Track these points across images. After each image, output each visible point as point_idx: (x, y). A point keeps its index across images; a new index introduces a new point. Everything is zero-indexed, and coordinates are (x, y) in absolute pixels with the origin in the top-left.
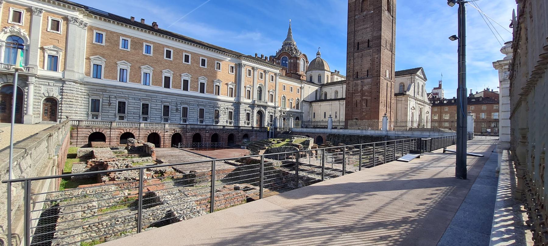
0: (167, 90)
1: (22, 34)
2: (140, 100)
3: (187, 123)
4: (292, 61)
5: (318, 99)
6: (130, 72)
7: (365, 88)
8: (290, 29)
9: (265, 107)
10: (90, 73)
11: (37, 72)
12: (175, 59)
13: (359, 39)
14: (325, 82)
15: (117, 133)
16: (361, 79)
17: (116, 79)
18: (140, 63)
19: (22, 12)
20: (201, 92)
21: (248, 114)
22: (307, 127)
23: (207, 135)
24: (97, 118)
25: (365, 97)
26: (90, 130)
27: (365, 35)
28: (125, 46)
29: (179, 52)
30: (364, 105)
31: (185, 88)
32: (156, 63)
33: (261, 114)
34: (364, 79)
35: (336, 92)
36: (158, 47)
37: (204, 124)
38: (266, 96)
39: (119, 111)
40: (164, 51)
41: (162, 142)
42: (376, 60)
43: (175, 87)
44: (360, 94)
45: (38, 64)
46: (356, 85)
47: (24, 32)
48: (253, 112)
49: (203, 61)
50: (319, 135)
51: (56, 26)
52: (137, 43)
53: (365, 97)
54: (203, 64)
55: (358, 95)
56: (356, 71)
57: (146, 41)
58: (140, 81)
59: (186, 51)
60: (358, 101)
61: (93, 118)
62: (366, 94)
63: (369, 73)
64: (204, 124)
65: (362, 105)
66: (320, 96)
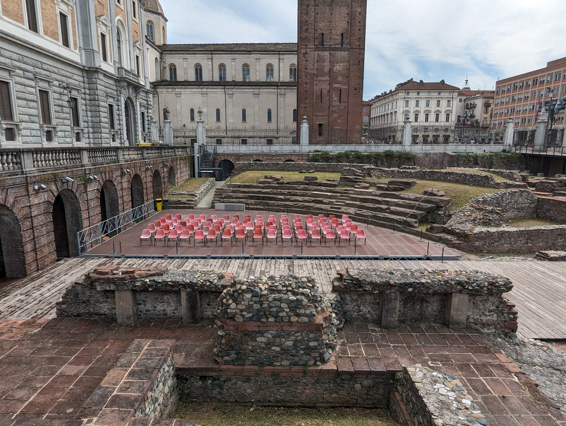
7: (338, 67)
13: (457, 300)
16: (330, 49)
25: (336, 85)
27: (423, 235)
30: (336, 98)
34: (336, 49)
35: (246, 68)
41: (28, 247)
42: (358, 18)
44: (327, 78)
46: (320, 60)
53: (336, 85)
55: (324, 79)
56: (319, 31)
60: (325, 92)
62: (340, 78)
63: (346, 41)
65: (330, 99)
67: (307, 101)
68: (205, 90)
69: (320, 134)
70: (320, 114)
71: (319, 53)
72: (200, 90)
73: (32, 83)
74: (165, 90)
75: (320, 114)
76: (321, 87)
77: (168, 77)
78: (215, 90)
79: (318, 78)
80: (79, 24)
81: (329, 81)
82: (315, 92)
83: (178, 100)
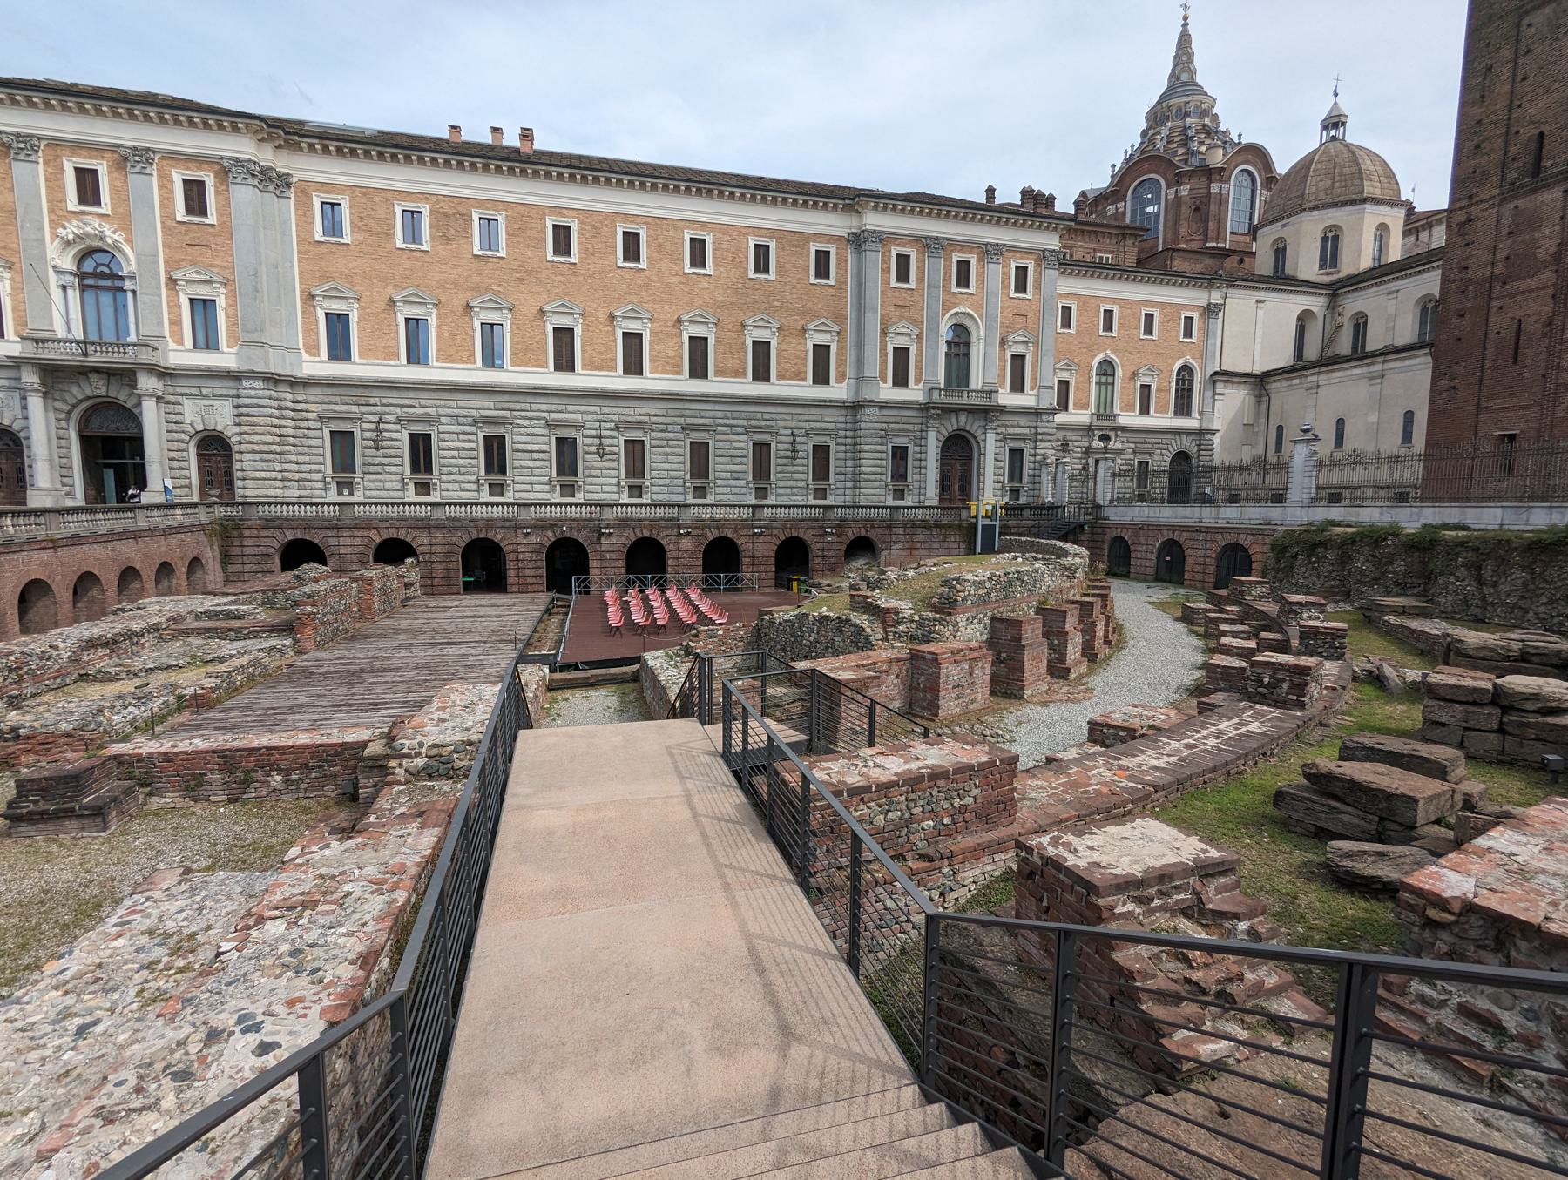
0: (760, 389)
1: (109, 241)
2: (475, 423)
3: (830, 501)
4: (1185, 190)
5: (1311, 353)
6: (439, 327)
8: (1184, 40)
9: (987, 413)
10: (317, 346)
11: (166, 359)
12: (586, 253)
14: (1366, 263)
15: (358, 541)
17: (397, 356)
18: (467, 289)
19: (100, 169)
20: (558, 368)
21: (900, 454)
22: (1233, 499)
23: (686, 544)
24: (351, 493)
26: (277, 533)
28: (413, 235)
29: (597, 222)
31: (761, 374)
32: (521, 280)
33: (959, 451)
36: (523, 217)
37: (509, 497)
38: (986, 369)
39: (415, 468)
40: (544, 231)
43: (592, 365)
44: (1548, 276)
45: (167, 334)
47: (112, 235)
48: (921, 442)
49: (698, 246)
50: (1230, 538)
51: (195, 197)
52: (452, 217)
54: (698, 259)
55: (1532, 283)
57: (481, 203)
58: (472, 354)
59: (692, 223)
60: (1533, 327)
61: (340, 493)
64: (509, 497)
66: (1328, 342)
67: (1461, 369)
68: (1378, 367)
69: (1508, 469)
70: (1508, 403)
71: (1520, 203)
72: (1365, 369)
73: (743, 438)
74: (1285, 384)
75: (1508, 403)
76: (1519, 314)
77: (1344, 346)
78: (1408, 362)
79: (1508, 287)
80: (570, 408)
81: (1554, 285)
82: (1492, 336)
83: (1311, 402)
